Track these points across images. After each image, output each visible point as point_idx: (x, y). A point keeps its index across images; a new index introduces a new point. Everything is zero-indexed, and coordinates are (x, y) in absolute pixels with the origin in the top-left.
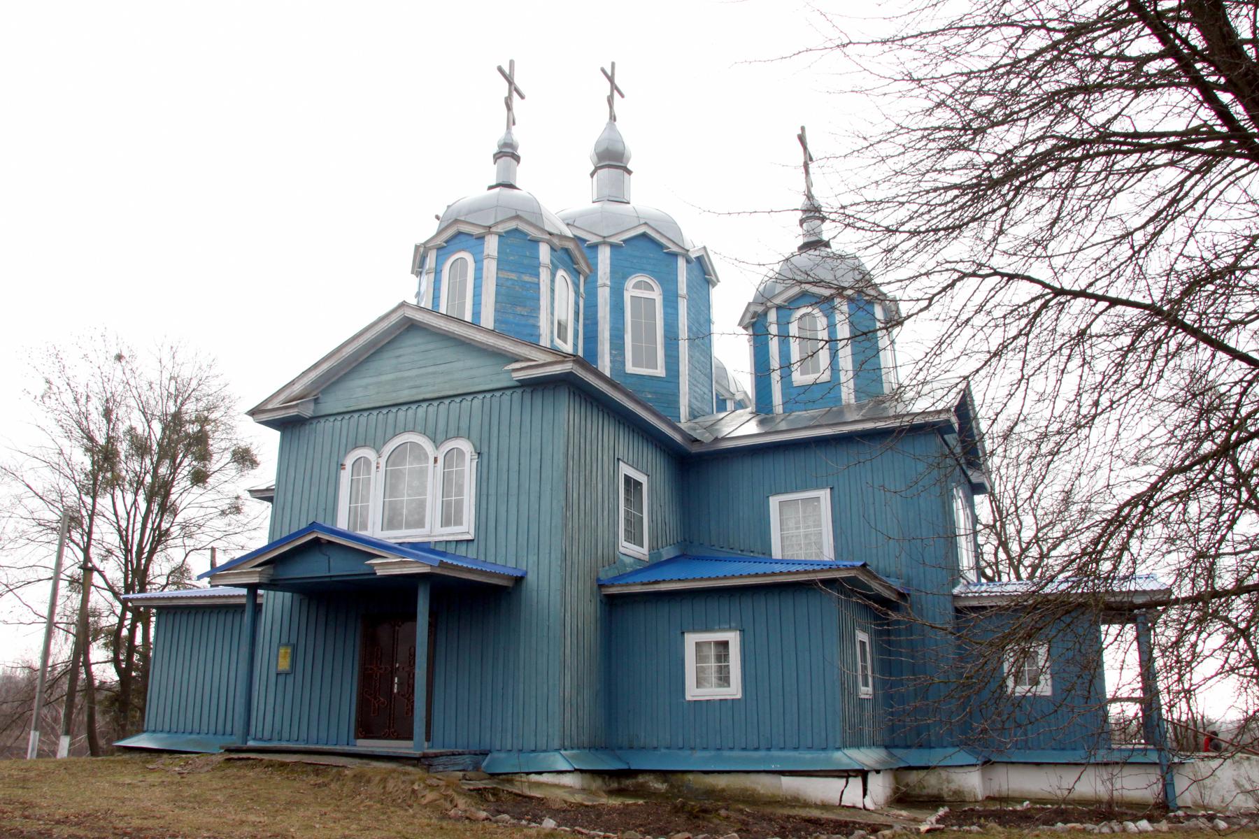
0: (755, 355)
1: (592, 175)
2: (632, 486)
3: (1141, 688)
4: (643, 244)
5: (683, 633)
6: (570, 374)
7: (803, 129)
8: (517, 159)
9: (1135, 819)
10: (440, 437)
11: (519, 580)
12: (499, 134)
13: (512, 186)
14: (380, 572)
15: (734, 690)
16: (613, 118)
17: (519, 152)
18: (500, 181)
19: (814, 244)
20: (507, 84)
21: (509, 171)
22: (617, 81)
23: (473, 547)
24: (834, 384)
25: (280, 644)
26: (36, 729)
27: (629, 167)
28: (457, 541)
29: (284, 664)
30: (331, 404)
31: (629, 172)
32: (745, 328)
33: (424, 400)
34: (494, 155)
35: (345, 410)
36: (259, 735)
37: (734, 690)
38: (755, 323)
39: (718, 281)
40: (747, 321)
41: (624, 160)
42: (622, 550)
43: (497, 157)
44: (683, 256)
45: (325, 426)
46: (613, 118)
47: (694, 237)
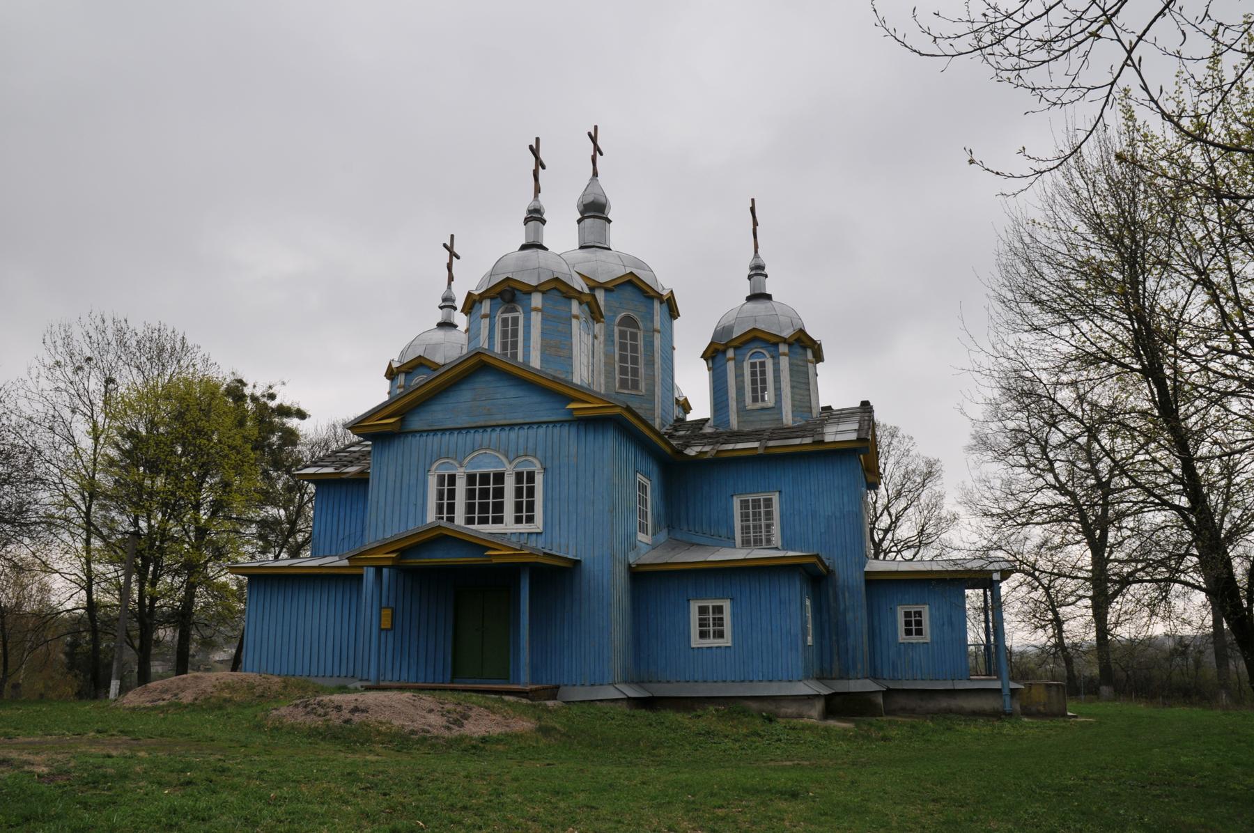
0: (713, 382)
1: (579, 221)
2: (643, 488)
3: (1061, 650)
4: (628, 293)
5: (689, 600)
6: (619, 415)
7: (753, 200)
8: (544, 222)
9: (1192, 522)
10: (512, 456)
11: (577, 563)
12: (527, 201)
13: (541, 247)
14: (495, 561)
15: (727, 641)
16: (595, 174)
17: (545, 216)
18: (531, 240)
19: (759, 296)
20: (534, 159)
21: (538, 233)
22: (599, 143)
23: (541, 540)
24: (778, 407)
25: (381, 608)
26: (117, 679)
27: (609, 217)
28: (528, 533)
29: (386, 624)
30: (416, 423)
31: (609, 221)
32: (706, 360)
33: (498, 426)
34: (526, 219)
35: (430, 428)
36: (365, 677)
37: (727, 641)
38: (713, 354)
39: (679, 316)
40: (708, 354)
41: (606, 212)
42: (639, 538)
43: (527, 221)
44: (658, 298)
45: (415, 442)
46: (595, 174)
47: (664, 281)
